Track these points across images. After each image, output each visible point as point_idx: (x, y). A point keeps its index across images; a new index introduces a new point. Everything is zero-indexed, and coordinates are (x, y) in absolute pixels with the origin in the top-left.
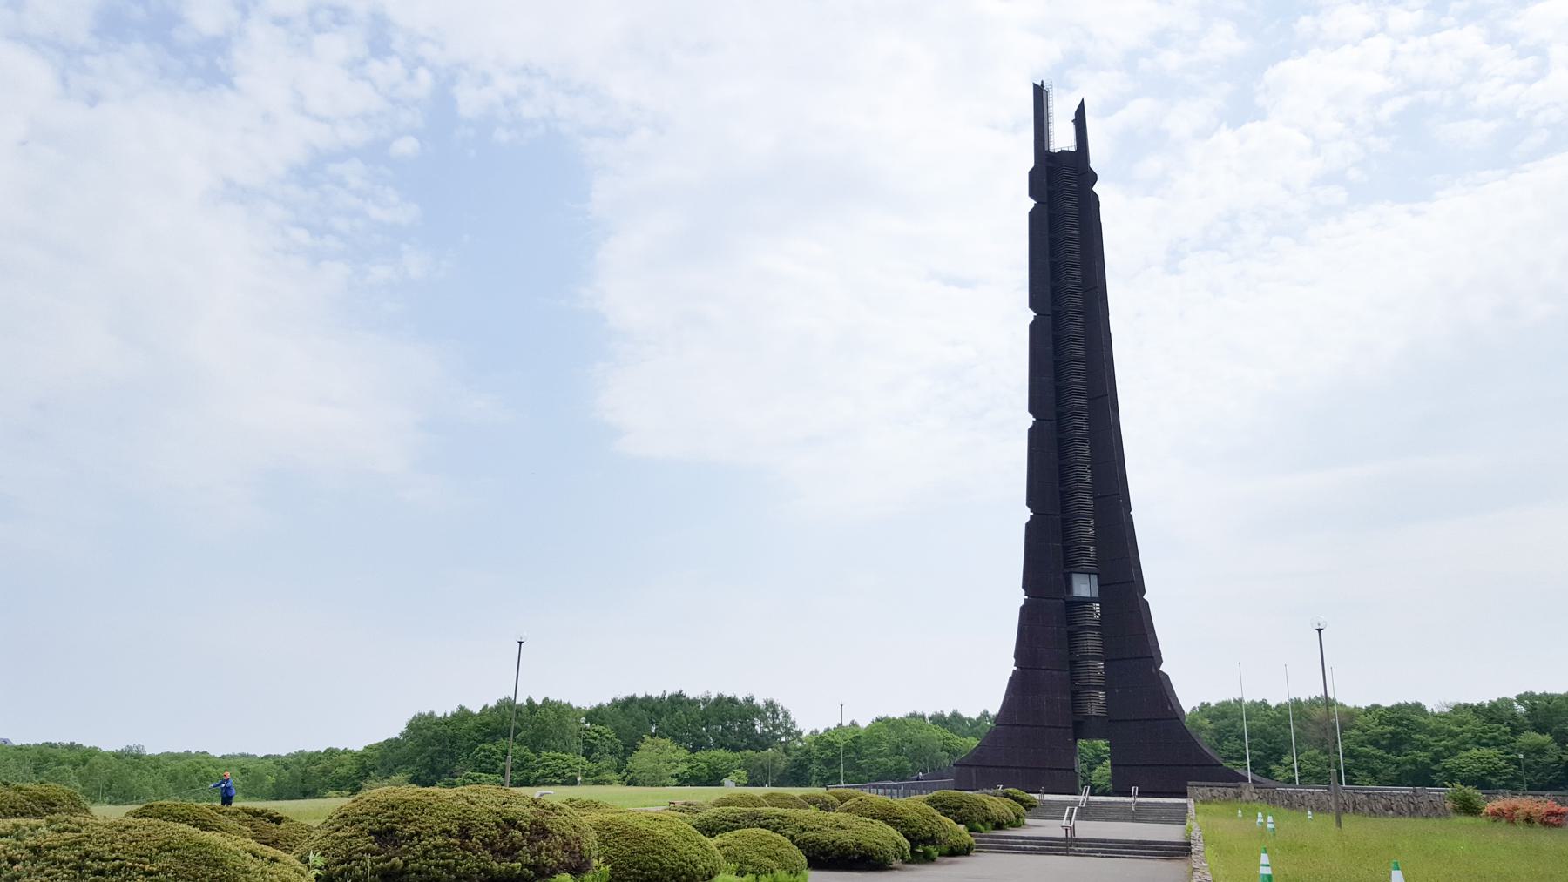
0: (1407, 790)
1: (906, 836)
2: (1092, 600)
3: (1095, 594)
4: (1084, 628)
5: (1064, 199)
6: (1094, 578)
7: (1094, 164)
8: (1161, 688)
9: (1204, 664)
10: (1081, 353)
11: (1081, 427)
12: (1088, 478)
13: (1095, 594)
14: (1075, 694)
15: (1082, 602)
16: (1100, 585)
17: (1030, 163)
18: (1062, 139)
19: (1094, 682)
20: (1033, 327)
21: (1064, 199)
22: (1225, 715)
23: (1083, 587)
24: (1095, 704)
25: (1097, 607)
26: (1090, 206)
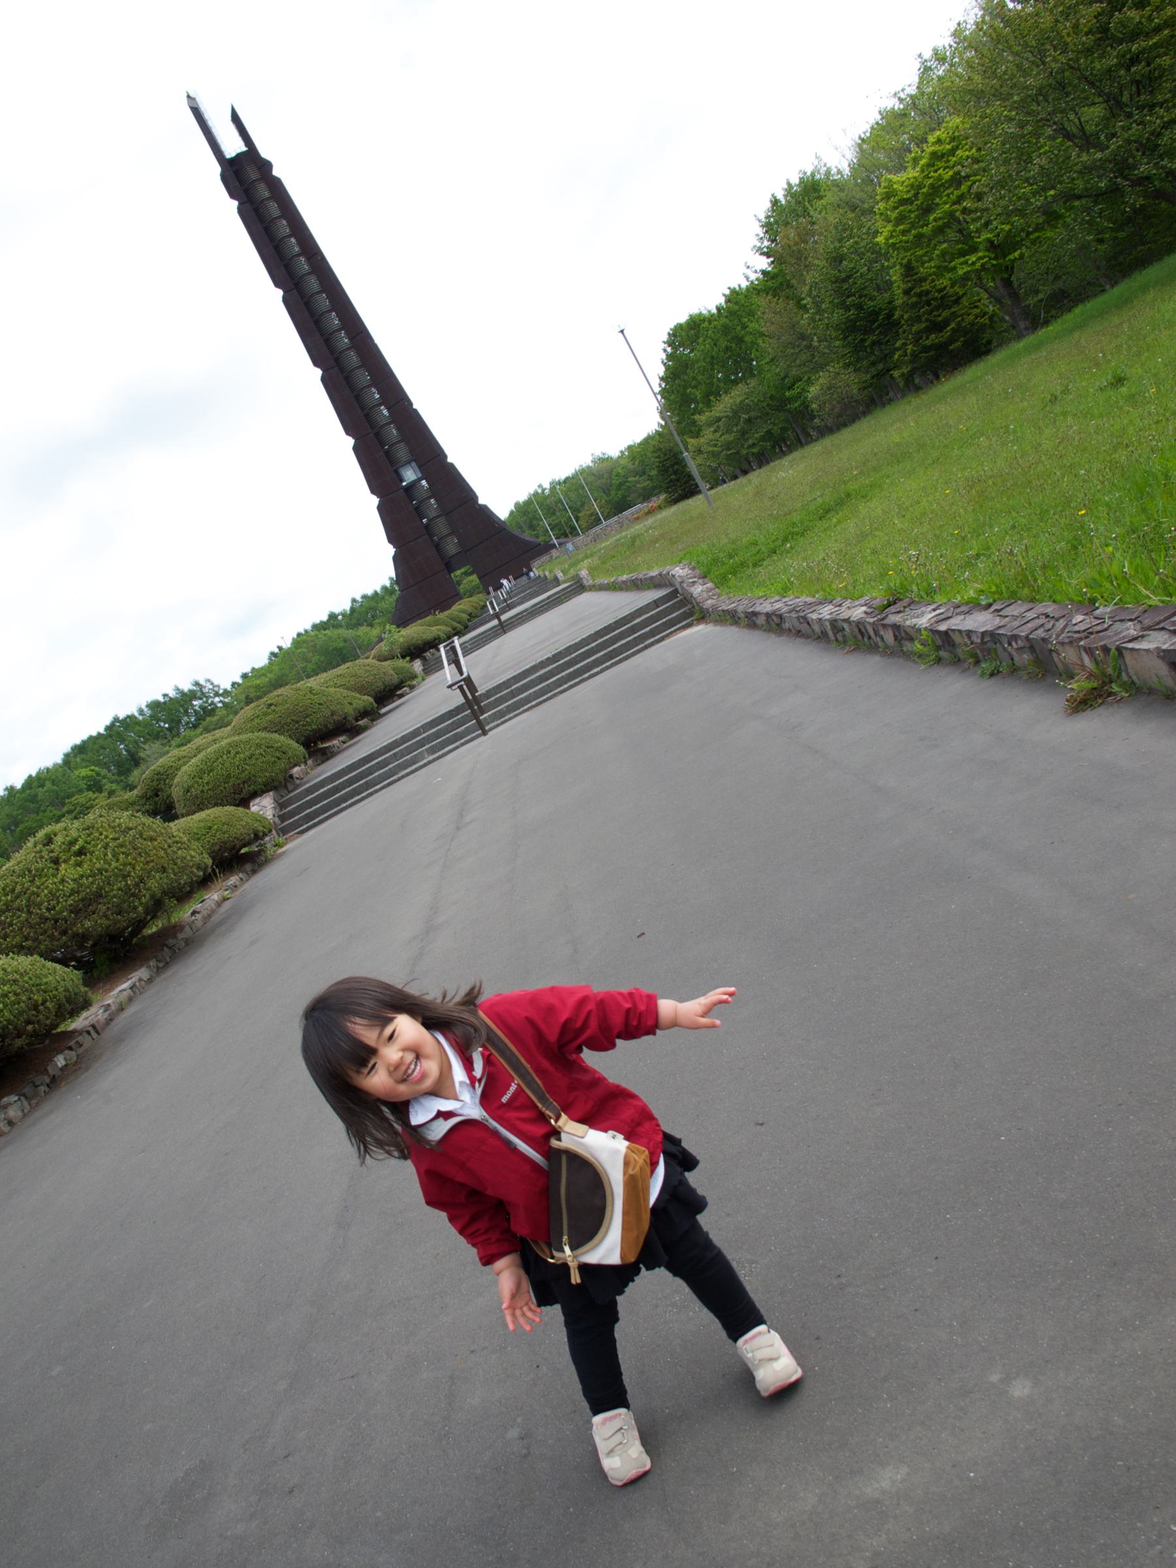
0: (616, 518)
1: (20, 949)
2: (420, 480)
3: (420, 475)
4: (322, 314)
5: (251, 182)
6: (414, 464)
7: (265, 152)
8: (485, 513)
9: (500, 491)
10: (267, 194)
11: (353, 358)
12: (377, 396)
13: (420, 475)
14: (437, 546)
15: (413, 485)
16: (419, 467)
17: (218, 169)
18: (233, 146)
19: (425, 495)
20: (285, 301)
21: (251, 182)
22: (524, 510)
23: (410, 475)
24: (452, 546)
25: (424, 482)
26: (277, 189)
